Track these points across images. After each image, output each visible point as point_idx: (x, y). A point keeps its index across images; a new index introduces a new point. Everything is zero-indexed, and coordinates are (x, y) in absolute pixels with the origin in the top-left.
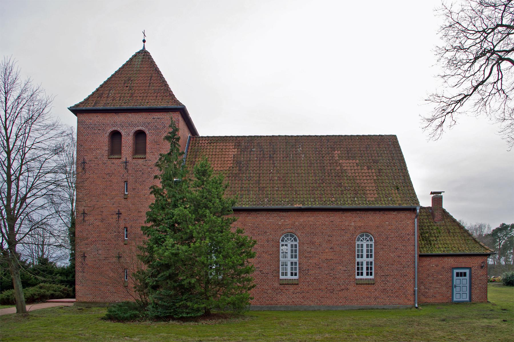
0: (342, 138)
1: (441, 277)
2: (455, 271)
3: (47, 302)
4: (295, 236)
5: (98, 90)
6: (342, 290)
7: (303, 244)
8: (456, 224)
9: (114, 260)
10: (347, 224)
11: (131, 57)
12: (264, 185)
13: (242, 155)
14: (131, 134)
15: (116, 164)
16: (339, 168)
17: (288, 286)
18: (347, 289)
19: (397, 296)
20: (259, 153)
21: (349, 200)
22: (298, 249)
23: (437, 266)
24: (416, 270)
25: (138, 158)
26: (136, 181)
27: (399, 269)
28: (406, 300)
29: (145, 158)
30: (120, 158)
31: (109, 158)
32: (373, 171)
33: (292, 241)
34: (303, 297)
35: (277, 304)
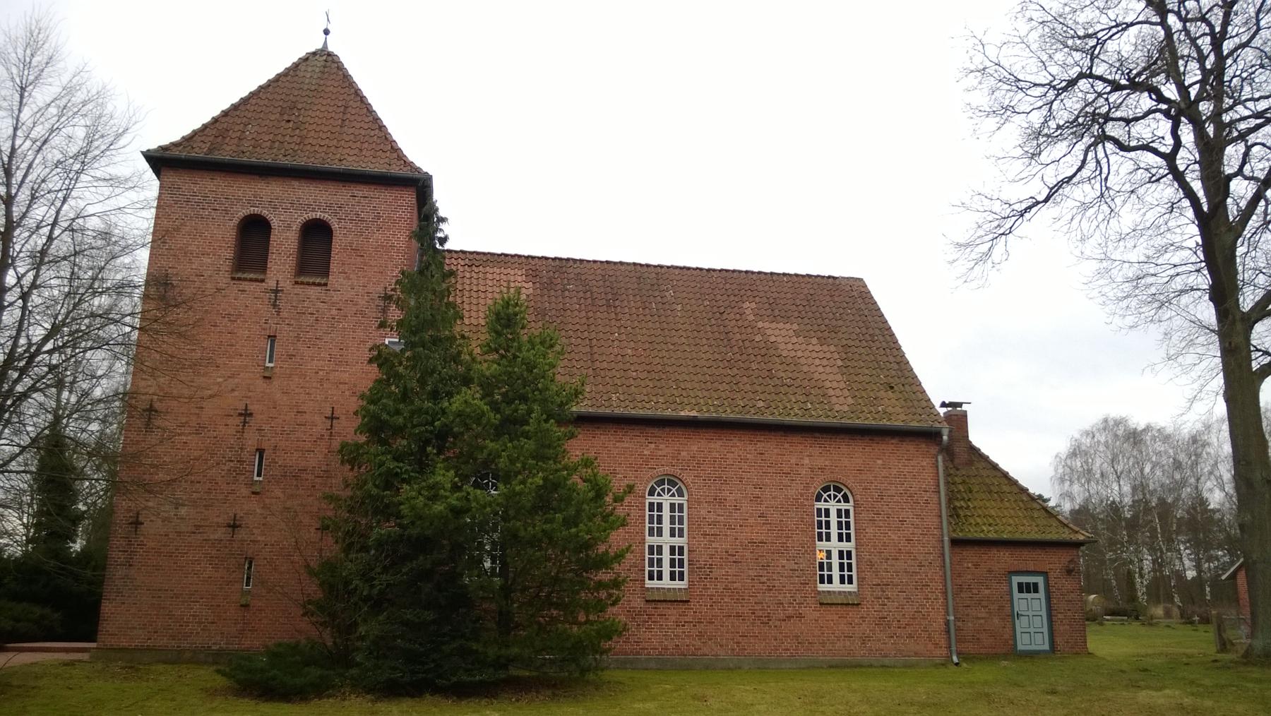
0: (754, 277)
1: (987, 592)
2: (1016, 580)
3: (8, 650)
4: (680, 484)
5: (215, 120)
6: (789, 617)
7: (699, 503)
8: (999, 474)
9: (220, 534)
10: (793, 461)
11: (295, 60)
12: (605, 365)
13: (546, 298)
14: (296, 227)
15: (250, 296)
16: (758, 338)
17: (664, 605)
18: (800, 616)
19: (910, 636)
20: (581, 294)
21: (796, 407)
22: (685, 514)
23: (976, 565)
24: (949, 573)
25: (308, 284)
26: (298, 338)
27: (912, 569)
28: (930, 646)
29: (326, 285)
30: (263, 281)
31: (233, 279)
32: (832, 348)
33: (673, 495)
34: (701, 635)
35: (638, 653)
